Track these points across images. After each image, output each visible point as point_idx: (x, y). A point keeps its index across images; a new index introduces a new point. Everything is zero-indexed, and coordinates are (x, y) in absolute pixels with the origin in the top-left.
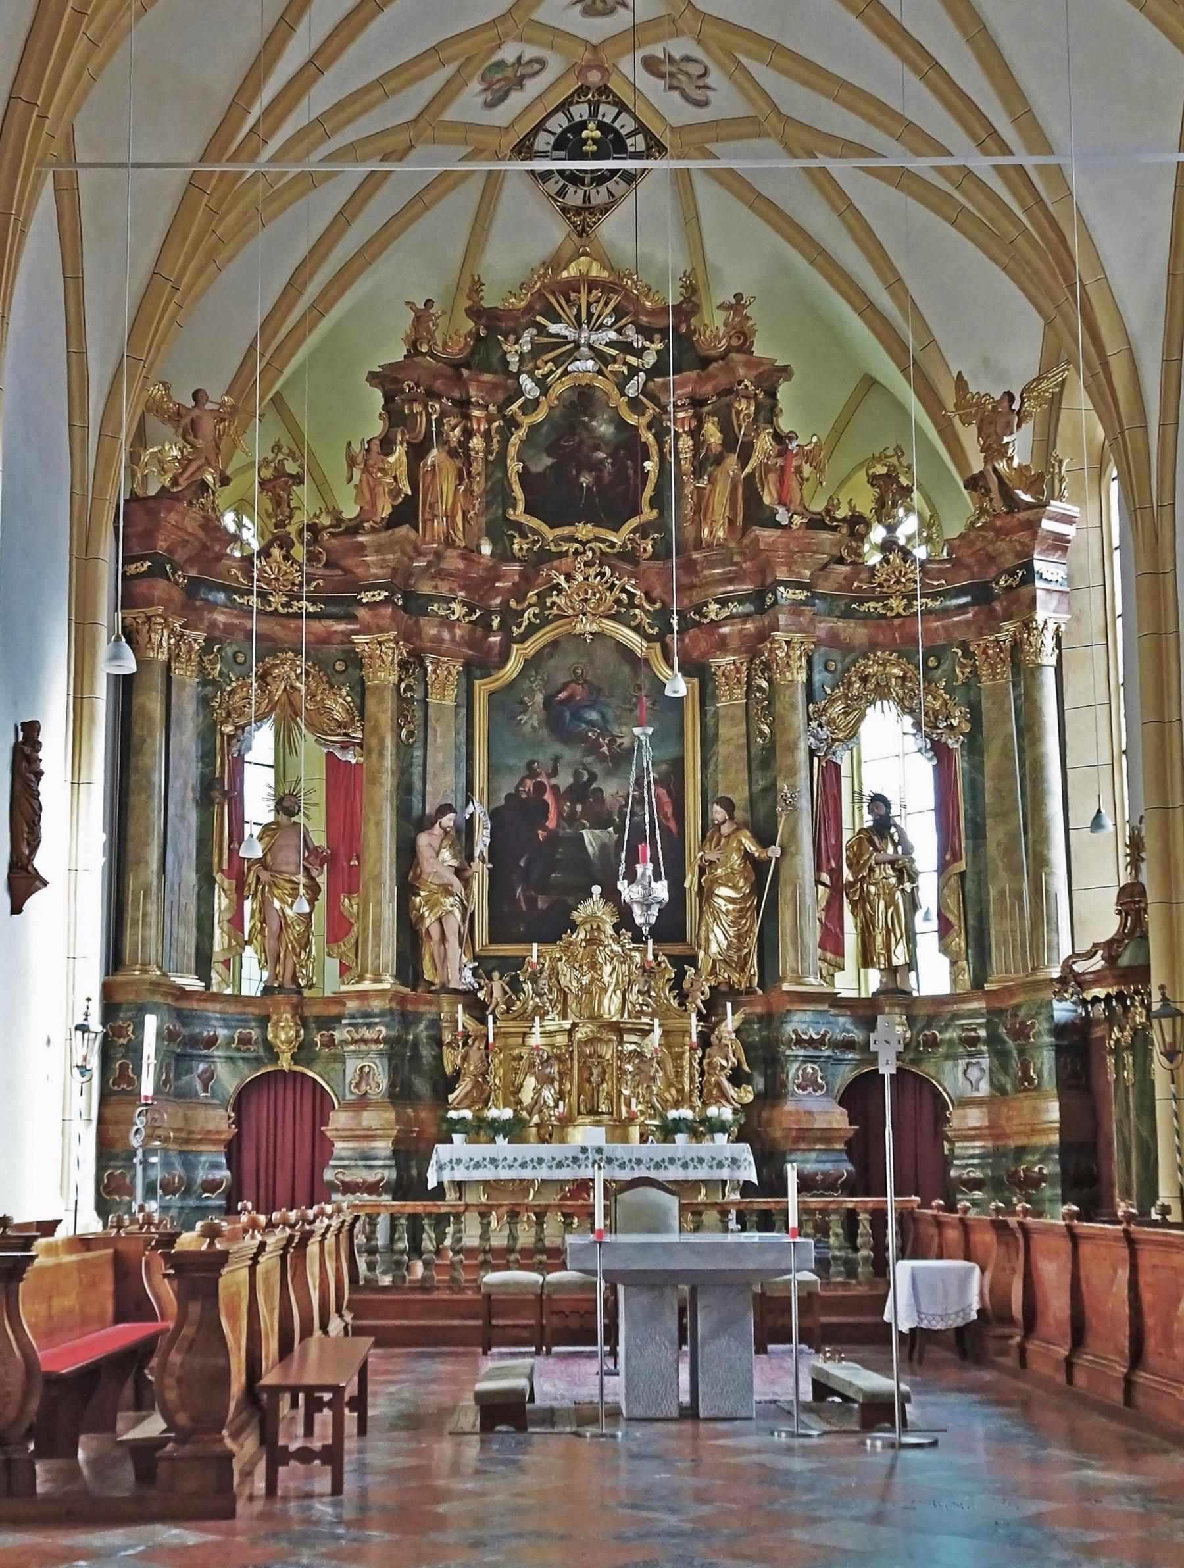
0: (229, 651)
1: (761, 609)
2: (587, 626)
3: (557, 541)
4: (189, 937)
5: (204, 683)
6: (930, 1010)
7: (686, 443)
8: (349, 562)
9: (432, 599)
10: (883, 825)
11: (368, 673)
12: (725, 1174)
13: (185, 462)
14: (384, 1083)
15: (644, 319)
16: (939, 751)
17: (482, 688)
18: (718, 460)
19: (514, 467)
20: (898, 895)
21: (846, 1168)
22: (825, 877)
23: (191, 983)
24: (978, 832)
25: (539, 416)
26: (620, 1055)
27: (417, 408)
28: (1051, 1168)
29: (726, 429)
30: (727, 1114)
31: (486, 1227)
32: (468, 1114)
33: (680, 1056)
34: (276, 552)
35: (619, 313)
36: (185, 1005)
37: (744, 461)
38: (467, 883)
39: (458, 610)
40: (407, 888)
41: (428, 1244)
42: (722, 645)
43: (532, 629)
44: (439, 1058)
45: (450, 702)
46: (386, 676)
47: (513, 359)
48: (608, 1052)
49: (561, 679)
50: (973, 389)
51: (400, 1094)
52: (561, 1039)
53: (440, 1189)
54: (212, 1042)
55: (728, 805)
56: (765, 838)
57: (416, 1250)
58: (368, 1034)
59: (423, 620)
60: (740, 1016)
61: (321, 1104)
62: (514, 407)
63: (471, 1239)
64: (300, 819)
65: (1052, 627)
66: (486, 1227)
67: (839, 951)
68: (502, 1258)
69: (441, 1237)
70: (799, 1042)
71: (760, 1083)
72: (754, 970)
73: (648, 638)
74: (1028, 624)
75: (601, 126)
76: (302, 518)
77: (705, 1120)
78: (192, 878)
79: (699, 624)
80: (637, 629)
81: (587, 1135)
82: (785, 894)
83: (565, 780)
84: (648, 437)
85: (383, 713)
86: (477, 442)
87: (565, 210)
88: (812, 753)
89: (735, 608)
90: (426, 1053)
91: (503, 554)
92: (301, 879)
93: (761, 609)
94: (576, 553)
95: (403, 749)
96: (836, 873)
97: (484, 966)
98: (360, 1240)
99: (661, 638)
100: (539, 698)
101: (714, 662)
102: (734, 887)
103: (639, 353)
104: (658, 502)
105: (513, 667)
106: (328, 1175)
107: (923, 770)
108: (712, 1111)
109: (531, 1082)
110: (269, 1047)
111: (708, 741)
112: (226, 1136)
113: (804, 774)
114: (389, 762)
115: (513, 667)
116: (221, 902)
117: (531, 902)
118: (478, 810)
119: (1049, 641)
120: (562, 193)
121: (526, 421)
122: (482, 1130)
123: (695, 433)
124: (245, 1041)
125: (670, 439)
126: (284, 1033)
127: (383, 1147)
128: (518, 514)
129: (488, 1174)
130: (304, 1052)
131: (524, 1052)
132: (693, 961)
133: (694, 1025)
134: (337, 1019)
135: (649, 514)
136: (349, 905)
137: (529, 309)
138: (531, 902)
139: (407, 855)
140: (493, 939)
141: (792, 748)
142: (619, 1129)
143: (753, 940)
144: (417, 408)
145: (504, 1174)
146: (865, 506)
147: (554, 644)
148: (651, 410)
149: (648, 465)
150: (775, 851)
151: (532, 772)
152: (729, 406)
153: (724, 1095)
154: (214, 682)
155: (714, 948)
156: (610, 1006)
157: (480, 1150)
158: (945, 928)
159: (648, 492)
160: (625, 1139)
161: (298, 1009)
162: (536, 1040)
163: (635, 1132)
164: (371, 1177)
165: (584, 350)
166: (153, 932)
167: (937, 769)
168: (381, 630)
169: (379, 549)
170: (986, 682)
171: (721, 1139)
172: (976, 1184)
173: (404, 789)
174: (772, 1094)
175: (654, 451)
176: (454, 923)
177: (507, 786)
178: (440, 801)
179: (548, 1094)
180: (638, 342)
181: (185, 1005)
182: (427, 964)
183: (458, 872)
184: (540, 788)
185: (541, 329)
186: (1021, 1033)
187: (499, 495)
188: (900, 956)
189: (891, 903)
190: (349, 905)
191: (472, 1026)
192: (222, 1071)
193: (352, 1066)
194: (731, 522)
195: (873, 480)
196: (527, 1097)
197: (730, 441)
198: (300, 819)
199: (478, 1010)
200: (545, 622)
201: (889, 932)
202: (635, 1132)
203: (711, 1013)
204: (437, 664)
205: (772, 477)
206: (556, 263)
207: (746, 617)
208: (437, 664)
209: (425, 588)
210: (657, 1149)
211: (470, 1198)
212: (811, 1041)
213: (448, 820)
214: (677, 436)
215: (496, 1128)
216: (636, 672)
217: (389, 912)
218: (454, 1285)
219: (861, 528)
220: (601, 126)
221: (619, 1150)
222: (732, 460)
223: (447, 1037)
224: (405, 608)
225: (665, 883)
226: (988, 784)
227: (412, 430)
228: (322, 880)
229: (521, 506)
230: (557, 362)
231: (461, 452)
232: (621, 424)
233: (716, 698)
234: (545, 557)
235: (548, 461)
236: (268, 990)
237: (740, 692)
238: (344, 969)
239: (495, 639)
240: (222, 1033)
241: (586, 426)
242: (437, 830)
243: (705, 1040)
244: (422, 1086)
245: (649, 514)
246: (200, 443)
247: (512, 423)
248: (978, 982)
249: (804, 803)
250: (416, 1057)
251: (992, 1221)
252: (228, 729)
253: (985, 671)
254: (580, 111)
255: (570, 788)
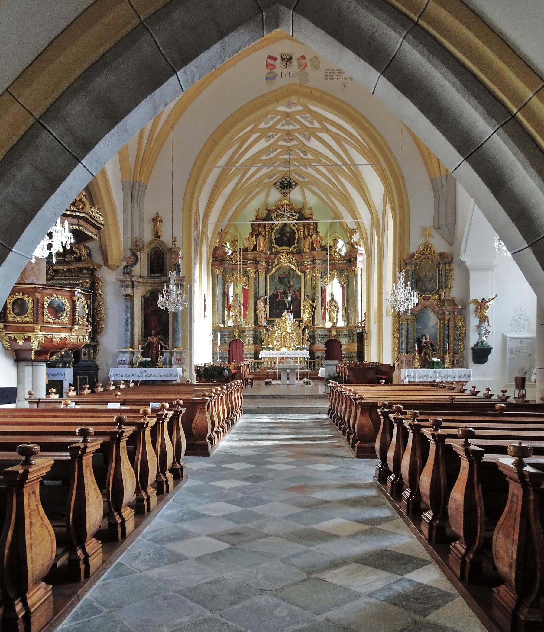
0: (227, 271)
1: (314, 263)
2: (286, 264)
3: (280, 250)
4: (221, 318)
5: (223, 276)
6: (340, 329)
7: (302, 233)
8: (246, 256)
9: (259, 261)
10: (333, 300)
11: (249, 275)
12: (305, 356)
13: (220, 242)
14: (252, 342)
15: (295, 210)
16: (343, 286)
17: (268, 275)
18: (307, 237)
19: (273, 237)
20: (335, 311)
21: (325, 355)
22: (323, 308)
23: (222, 326)
24: (348, 300)
25: (278, 227)
26: (289, 337)
27: (257, 228)
28: (355, 355)
29: (309, 232)
30: (306, 347)
31: (267, 364)
32: (265, 346)
33: (299, 337)
34: (234, 254)
35: (291, 209)
36: (221, 329)
37: (311, 238)
38: (265, 308)
39: (264, 263)
40: (256, 310)
41: (259, 366)
42: (307, 269)
43: (276, 265)
44: (261, 337)
45: (262, 278)
46: (252, 275)
47: (273, 218)
48: (288, 337)
49: (281, 273)
50: (349, 226)
51: (255, 343)
52: (280, 335)
53: (261, 359)
54: (225, 335)
55: (308, 296)
56: (313, 302)
57: (258, 367)
58: (250, 334)
59: (258, 265)
60: (309, 331)
61: (242, 345)
62: (273, 226)
63: (266, 366)
64: (239, 298)
65: (360, 268)
66: (267, 364)
67: (325, 320)
68: (270, 368)
69: (261, 365)
70: (318, 335)
71: (312, 341)
72: (311, 323)
73: (296, 267)
74: (356, 267)
75: (287, 181)
76: (238, 247)
77: (302, 348)
78: (222, 308)
79: (304, 265)
80: (294, 265)
81: (284, 350)
82: (316, 311)
83: (282, 291)
84: (296, 231)
85: (252, 281)
86: (267, 233)
87: (282, 193)
88: (321, 287)
89: (310, 263)
90: (259, 336)
91: (272, 253)
92: (239, 308)
93: (314, 263)
94: (284, 252)
95: (255, 286)
96: (325, 307)
97: (269, 322)
98: (250, 366)
99: (297, 267)
100: (277, 277)
101: (306, 271)
102: (309, 310)
103: (295, 216)
104: (297, 243)
105: (273, 271)
106: (244, 356)
107: (340, 289)
108: (303, 346)
109: (275, 342)
110: (234, 335)
111: (305, 284)
112: (228, 350)
113: (320, 291)
114: (253, 289)
115: (273, 271)
116: (226, 312)
117: (276, 311)
118: (267, 297)
119: (359, 270)
120: (281, 191)
121: (275, 229)
122: (268, 349)
123: (304, 231)
124: (230, 335)
125: (299, 232)
126: (236, 333)
127: (252, 351)
128: (274, 245)
129: (268, 356)
130: (240, 336)
131: (274, 337)
132: (301, 321)
133: (301, 332)
134: (245, 331)
135: (296, 245)
136: (246, 312)
137: (276, 209)
138: (276, 311)
139: (256, 304)
140: (270, 317)
141: (318, 287)
142: (289, 349)
143: (311, 318)
144: (257, 228)
145: (271, 356)
146: (332, 245)
147: (280, 267)
148: (297, 226)
149: (296, 236)
150: (315, 304)
151: (276, 290)
152: (309, 227)
153: (306, 343)
154: (224, 276)
155: (305, 320)
156: (288, 330)
157: (267, 352)
158: (343, 316)
159: (296, 241)
160: (290, 350)
161: (238, 329)
162: (276, 335)
163: (291, 349)
164: (251, 356)
165: (285, 216)
166: (216, 318)
167: (342, 290)
168: (252, 267)
169: (251, 254)
170: (350, 276)
171: (305, 350)
172: (345, 357)
173: (255, 293)
174: (313, 343)
175: (297, 234)
176: (263, 315)
177: (272, 292)
178: (261, 295)
179: (278, 343)
180: (294, 214)
181: (221, 329)
182: (259, 322)
183: (264, 307)
184: (277, 292)
185: (278, 212)
186: (352, 334)
187: (271, 242)
188: (335, 321)
189: (334, 312)
190: (246, 312)
191: (266, 332)
192: (227, 339)
193: (247, 339)
194: (309, 249)
195: (333, 240)
196: (275, 344)
197: (309, 234)
198: (239, 298)
199: (267, 330)
200: (278, 264)
201: (333, 317)
202: (291, 349)
203: (304, 331)
204: (260, 272)
205: (315, 242)
206: (280, 201)
207: (311, 264)
208: (260, 272)
209: (258, 259)
210: (295, 352)
211: (266, 360)
212: (320, 335)
213: (262, 298)
214: (301, 232)
215: (270, 349)
216: (293, 272)
217: (253, 314)
218: (263, 372)
219: (331, 248)
220: (287, 181)
221: (289, 352)
222: (309, 237)
223: (262, 334)
224: (255, 263)
225: (292, 316)
226: (350, 293)
227: (256, 232)
228: (242, 309)
229: (274, 243)
230: (281, 218)
231: (265, 236)
232: (292, 229)
233: (307, 277)
234: (278, 253)
235: (279, 236)
236: (234, 326)
237: (310, 276)
238: (246, 323)
239: (270, 267)
240: (227, 333)
241: (285, 229)
242: (260, 300)
243: (303, 335)
244: (258, 342)
245: (296, 245)
246: (222, 238)
247: (273, 229)
248: (347, 325)
249: (320, 296)
250: (257, 337)
251: (109, 379)
252: (227, 284)
253: (350, 274)
254: (284, 179)
255: (283, 292)
